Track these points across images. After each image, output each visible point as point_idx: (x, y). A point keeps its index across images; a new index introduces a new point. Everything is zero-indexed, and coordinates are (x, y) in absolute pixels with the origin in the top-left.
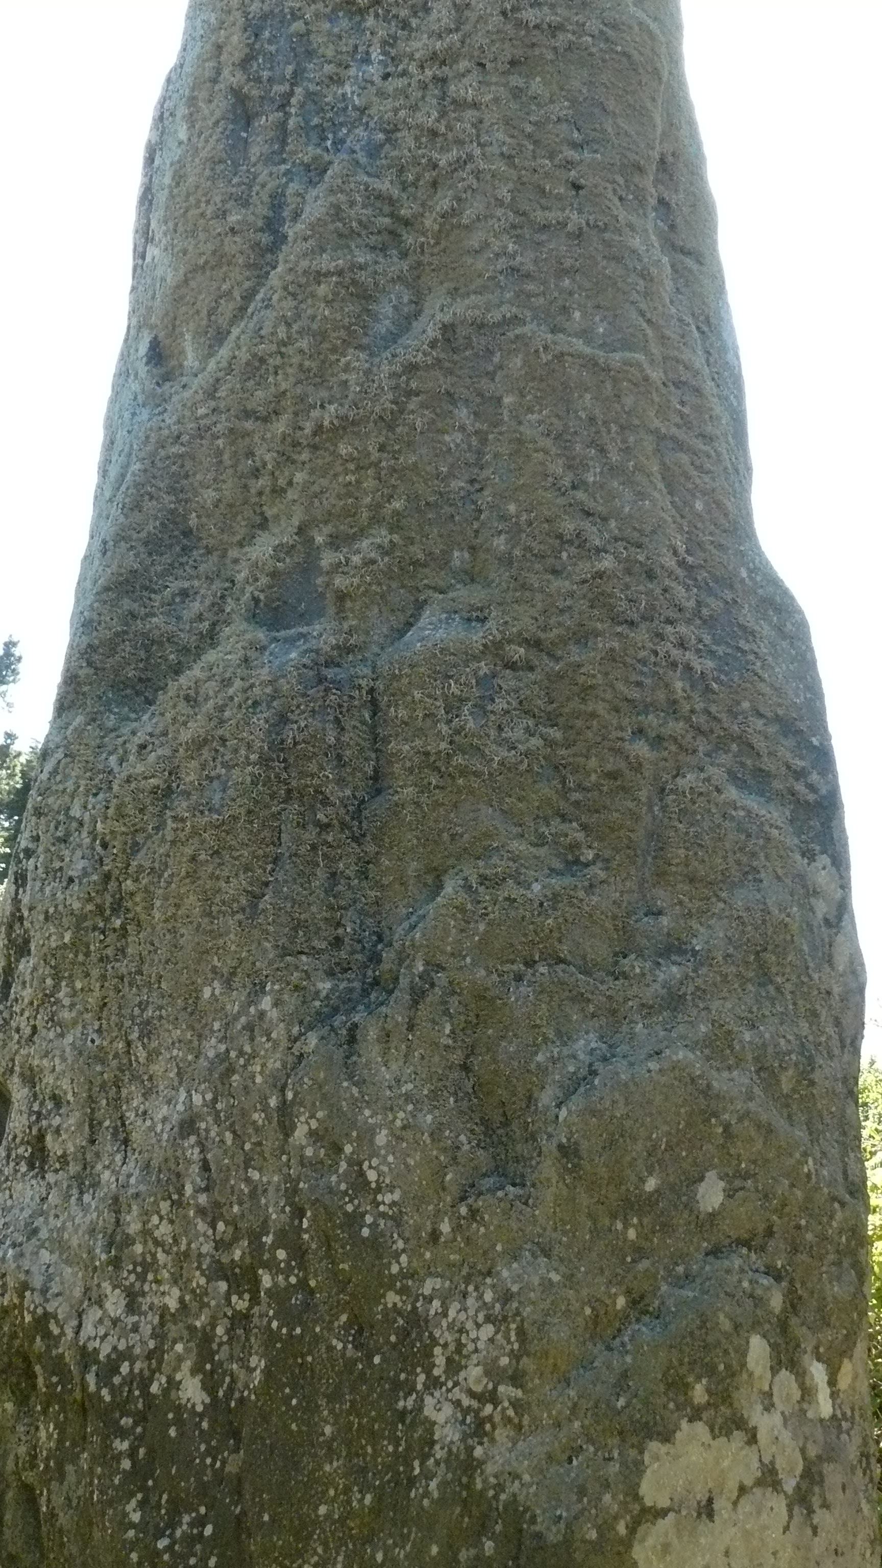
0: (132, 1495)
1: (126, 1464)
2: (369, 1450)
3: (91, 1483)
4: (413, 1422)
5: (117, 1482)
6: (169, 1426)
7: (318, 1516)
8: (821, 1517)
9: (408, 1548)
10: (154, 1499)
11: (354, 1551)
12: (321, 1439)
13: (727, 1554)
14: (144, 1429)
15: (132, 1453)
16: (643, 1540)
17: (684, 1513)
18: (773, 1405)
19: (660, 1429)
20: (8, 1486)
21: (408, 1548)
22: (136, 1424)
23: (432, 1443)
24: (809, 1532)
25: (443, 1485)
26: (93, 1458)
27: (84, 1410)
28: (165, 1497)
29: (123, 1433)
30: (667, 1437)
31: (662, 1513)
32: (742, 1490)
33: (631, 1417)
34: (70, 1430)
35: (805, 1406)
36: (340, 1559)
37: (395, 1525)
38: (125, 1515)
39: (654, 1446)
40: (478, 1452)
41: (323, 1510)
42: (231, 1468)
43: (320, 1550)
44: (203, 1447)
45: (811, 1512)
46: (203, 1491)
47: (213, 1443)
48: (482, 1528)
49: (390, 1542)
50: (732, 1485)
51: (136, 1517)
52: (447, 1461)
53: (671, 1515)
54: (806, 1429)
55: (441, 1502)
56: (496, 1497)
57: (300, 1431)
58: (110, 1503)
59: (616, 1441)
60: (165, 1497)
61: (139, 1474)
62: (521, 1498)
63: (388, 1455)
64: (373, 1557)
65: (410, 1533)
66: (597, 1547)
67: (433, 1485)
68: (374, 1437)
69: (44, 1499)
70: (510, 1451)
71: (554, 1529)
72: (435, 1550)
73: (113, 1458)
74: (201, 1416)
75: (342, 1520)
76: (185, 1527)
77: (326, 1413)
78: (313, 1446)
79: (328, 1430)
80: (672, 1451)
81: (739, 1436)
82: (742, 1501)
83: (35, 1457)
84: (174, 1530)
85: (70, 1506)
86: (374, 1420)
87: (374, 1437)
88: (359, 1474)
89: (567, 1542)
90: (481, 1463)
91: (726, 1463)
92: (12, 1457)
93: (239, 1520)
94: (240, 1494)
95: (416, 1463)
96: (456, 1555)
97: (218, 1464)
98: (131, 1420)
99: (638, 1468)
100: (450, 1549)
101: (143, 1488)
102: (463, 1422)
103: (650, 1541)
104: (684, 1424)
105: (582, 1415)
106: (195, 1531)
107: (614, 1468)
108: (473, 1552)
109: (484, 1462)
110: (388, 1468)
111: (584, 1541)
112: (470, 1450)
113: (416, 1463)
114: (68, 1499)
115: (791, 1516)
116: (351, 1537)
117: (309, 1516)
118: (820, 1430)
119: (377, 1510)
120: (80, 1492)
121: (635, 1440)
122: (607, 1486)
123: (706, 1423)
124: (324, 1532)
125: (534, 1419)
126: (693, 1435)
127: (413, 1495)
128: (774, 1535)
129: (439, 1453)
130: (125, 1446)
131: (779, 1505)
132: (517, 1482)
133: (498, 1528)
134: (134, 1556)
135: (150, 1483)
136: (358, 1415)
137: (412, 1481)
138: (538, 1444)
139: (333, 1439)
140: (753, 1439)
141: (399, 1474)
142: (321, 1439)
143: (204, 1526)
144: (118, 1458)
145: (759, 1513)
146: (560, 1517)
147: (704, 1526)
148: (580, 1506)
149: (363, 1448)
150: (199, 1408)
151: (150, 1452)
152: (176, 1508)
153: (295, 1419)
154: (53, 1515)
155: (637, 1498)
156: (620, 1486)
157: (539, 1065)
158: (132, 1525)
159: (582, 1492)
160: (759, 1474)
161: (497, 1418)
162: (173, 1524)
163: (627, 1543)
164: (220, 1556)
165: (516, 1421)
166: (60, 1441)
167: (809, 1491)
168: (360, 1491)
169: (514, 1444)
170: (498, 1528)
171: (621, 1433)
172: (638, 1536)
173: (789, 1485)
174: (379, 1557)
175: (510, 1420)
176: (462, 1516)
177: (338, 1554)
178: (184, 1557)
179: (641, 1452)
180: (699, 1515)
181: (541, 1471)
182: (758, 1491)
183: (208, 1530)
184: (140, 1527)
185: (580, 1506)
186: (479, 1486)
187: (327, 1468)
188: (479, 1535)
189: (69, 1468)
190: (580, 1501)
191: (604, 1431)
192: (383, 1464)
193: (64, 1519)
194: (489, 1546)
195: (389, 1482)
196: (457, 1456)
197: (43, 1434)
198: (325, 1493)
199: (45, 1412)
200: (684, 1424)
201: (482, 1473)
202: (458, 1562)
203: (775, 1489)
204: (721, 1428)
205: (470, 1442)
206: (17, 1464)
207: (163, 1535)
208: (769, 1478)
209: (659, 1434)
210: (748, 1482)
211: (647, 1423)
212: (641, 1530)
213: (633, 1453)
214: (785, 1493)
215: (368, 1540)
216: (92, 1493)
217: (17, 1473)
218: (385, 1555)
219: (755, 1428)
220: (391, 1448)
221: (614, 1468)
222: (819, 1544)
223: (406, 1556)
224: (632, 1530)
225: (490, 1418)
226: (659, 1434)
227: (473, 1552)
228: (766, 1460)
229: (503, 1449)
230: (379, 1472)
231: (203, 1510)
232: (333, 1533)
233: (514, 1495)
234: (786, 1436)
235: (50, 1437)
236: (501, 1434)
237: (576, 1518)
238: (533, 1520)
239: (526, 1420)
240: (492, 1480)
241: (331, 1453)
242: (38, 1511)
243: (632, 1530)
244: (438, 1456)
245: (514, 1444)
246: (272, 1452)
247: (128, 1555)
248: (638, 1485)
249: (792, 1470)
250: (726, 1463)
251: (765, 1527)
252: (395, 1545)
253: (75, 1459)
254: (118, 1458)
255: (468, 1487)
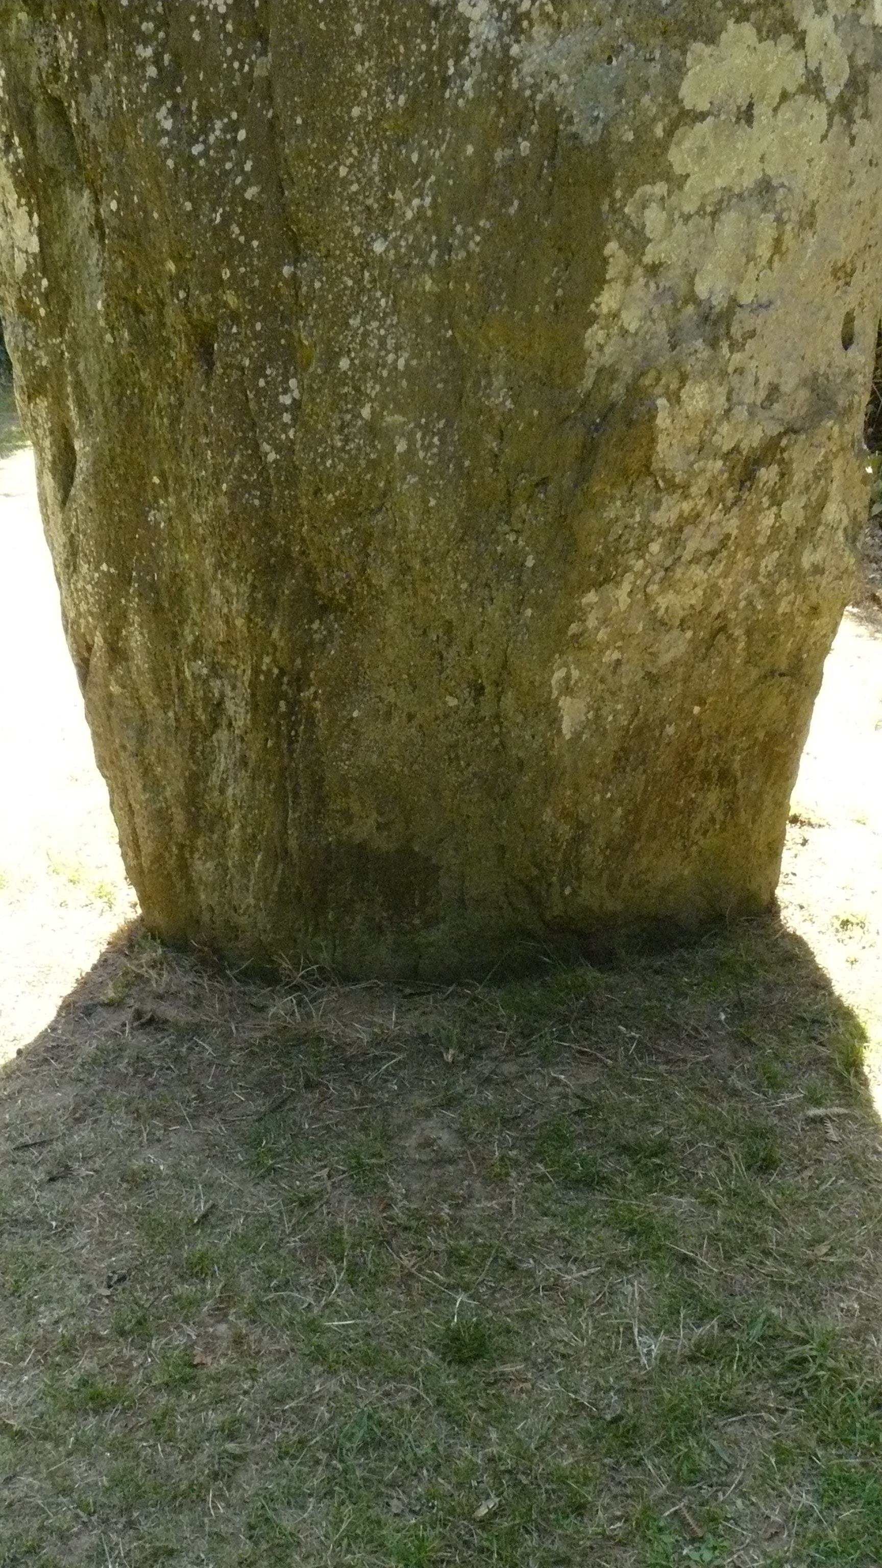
0: (161, 102)
1: (152, 71)
2: (402, 49)
3: (119, 93)
4: (447, 19)
5: (144, 90)
6: (192, 30)
7: (351, 118)
8: (861, 127)
9: (443, 148)
10: (183, 106)
11: (390, 152)
12: (352, 38)
13: (762, 159)
14: (167, 34)
15: (157, 60)
16: (678, 144)
17: (723, 117)
18: (825, 8)
19: (704, 28)
20: (35, 100)
21: (443, 148)
22: (158, 29)
23: (466, 41)
24: (847, 141)
25: (478, 84)
26: (117, 65)
27: (102, 18)
28: (195, 103)
29: (146, 40)
30: (711, 39)
31: (702, 116)
32: (785, 96)
33: (675, 16)
34: (90, 39)
35: (860, 10)
36: (375, 160)
37: (429, 125)
38: (157, 123)
39: (697, 47)
40: (515, 50)
41: (356, 111)
42: (260, 72)
43: (355, 152)
44: (229, 51)
45: (851, 121)
46: (233, 96)
47: (240, 46)
48: (518, 128)
49: (425, 142)
50: (774, 91)
51: (168, 124)
52: (482, 60)
53: (710, 119)
54: (858, 36)
55: (478, 100)
56: (532, 97)
57: (329, 30)
58: (140, 112)
59: (659, 40)
60: (195, 103)
61: (166, 81)
62: (558, 98)
63: (422, 54)
64: (408, 158)
65: (444, 134)
66: (633, 149)
67: (468, 84)
68: (406, 35)
69: (73, 111)
70: (547, 49)
71: (591, 129)
72: (470, 150)
73: (137, 66)
74: (225, 17)
75: (377, 121)
76: (218, 133)
77: (355, 10)
78: (342, 44)
79: (358, 28)
80: (716, 53)
81: (787, 40)
82: (784, 107)
83: (58, 69)
84: (207, 136)
85: (100, 116)
86: (406, 16)
87: (406, 35)
88: (392, 74)
89: (604, 143)
90: (518, 62)
91: (770, 68)
92: (34, 69)
93: (272, 124)
94: (271, 99)
95: (451, 63)
96: (491, 154)
97: (246, 68)
98: (151, 25)
99: (680, 69)
100: (485, 150)
101: (173, 96)
102: (499, 19)
103: (687, 144)
104: (731, 24)
105: (624, 12)
106: (229, 137)
107: (655, 69)
108: (508, 152)
109: (521, 61)
110: (421, 67)
111: (620, 142)
112: (506, 48)
113: (451, 63)
114: (97, 109)
115: (830, 125)
116: (385, 138)
117: (342, 118)
118: (871, 38)
119: (411, 110)
120: (109, 102)
121: (677, 40)
122: (646, 87)
123: (754, 24)
124: (359, 133)
125: (573, 16)
126: (739, 37)
127: (447, 95)
128: (812, 143)
129: (474, 51)
130: (148, 52)
131: (820, 112)
132: (554, 82)
133: (534, 128)
134: (170, 163)
135: (179, 90)
136: (389, 13)
137: (446, 82)
138: (577, 42)
139: (363, 38)
140: (800, 44)
141: (433, 73)
142: (352, 38)
143: (236, 131)
144: (142, 65)
145: (798, 121)
146: (597, 118)
147: (742, 131)
148: (617, 107)
149: (395, 47)
150: (222, 9)
151: (176, 56)
152: (207, 114)
153: (322, 17)
154: (84, 126)
155: (677, 101)
156: (661, 89)
157: (784, 614)
158: (165, 133)
159: (620, 92)
160: (803, 80)
161: (535, 14)
162: (205, 130)
163: (663, 146)
164: (257, 160)
165: (555, 17)
166: (81, 51)
167: (853, 101)
168: (394, 92)
169: (552, 43)
170: (534, 128)
171: (664, 33)
172: (675, 139)
173: (833, 93)
174: (415, 157)
175: (548, 16)
176: (498, 116)
177: (373, 155)
178: (220, 162)
179: (684, 53)
180: (738, 120)
181: (579, 71)
182: (800, 98)
183: (242, 135)
184: (174, 134)
185: (617, 107)
186: (515, 86)
187: (359, 68)
188: (515, 135)
189: (95, 79)
190: (618, 102)
191: (646, 30)
192: (417, 64)
193: (96, 131)
194: (525, 146)
195: (422, 82)
196: (493, 55)
197: (62, 44)
198: (356, 95)
199: (60, 20)
200: (731, 24)
201: (519, 71)
202: (494, 162)
203: (817, 97)
204: (768, 32)
205: (506, 39)
206: (40, 77)
207: (197, 142)
208: (813, 85)
209: (704, 35)
210: (791, 89)
211: (692, 22)
212: (678, 133)
213: (675, 54)
214: (828, 102)
215: (402, 141)
216: (121, 102)
217: (42, 86)
218: (420, 156)
219: (804, 32)
220: (424, 47)
221: (655, 69)
222: (854, 154)
223: (441, 157)
224: (670, 133)
225: (527, 15)
226: (704, 35)
227: (508, 152)
228: (812, 66)
229: (541, 47)
230: (413, 72)
231: (234, 115)
232: (367, 135)
233: (551, 96)
234: (835, 42)
235: (70, 46)
236: (540, 31)
237: (614, 118)
238: (570, 121)
239: (565, 17)
240: (529, 80)
241: (362, 53)
242: (68, 124)
243: (670, 133)
244: (473, 55)
245: (553, 43)
246: (301, 54)
247: (164, 162)
248: (678, 87)
249: (837, 77)
250: (770, 68)
251: (803, 135)
252: (430, 145)
253: (99, 69)
254: (142, 65)
255: (504, 86)
